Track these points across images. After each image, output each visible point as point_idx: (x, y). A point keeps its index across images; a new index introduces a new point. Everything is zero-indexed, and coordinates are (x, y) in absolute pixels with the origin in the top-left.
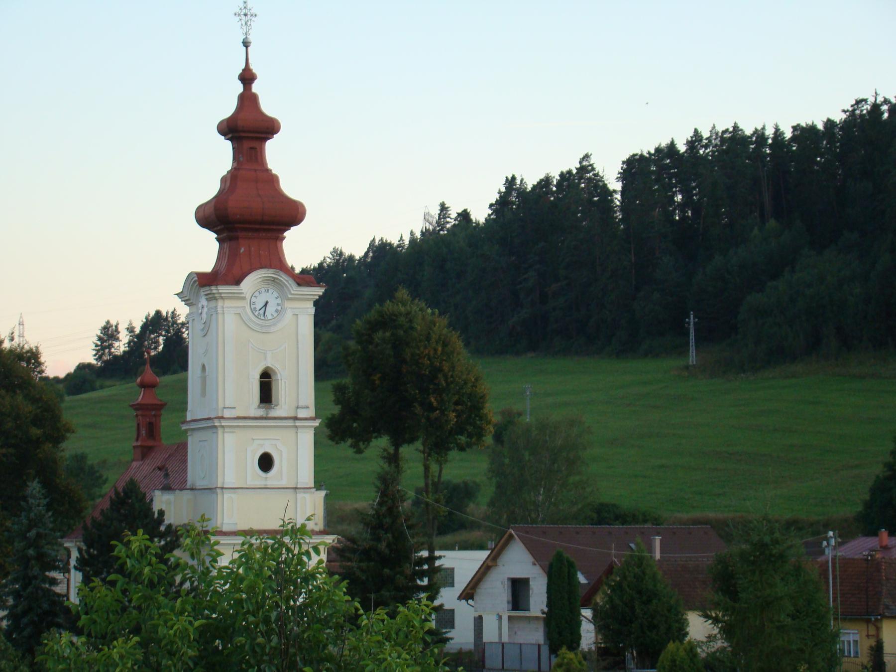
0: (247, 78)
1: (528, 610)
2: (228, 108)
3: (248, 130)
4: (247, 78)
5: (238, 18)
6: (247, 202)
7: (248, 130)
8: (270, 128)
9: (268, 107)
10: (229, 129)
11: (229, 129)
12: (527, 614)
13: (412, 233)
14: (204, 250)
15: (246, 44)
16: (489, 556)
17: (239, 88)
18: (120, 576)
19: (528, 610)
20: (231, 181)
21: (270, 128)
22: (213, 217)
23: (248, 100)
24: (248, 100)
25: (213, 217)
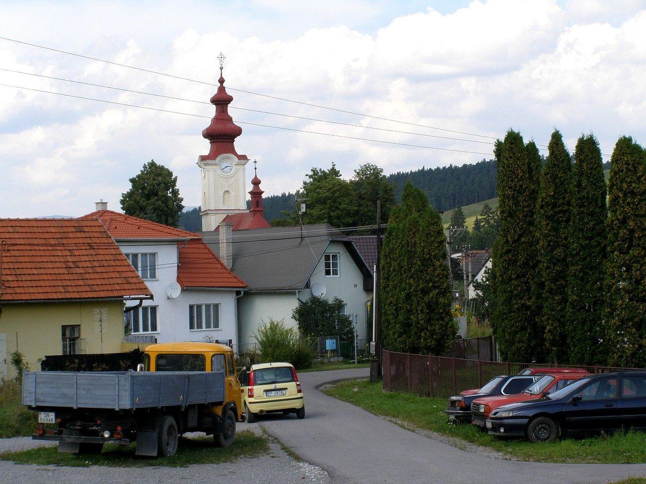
0: (222, 81)
1: (156, 330)
2: (214, 91)
3: (222, 101)
4: (222, 81)
5: (218, 59)
6: (221, 127)
7: (222, 101)
8: (230, 99)
9: (229, 92)
10: (215, 101)
11: (215, 101)
12: (156, 332)
13: (557, 139)
14: (205, 147)
15: (221, 69)
16: (116, 214)
17: (219, 85)
18: (605, 178)
19: (156, 330)
20: (216, 120)
21: (230, 99)
22: (209, 134)
23: (222, 89)
24: (222, 89)
25: (209, 134)
